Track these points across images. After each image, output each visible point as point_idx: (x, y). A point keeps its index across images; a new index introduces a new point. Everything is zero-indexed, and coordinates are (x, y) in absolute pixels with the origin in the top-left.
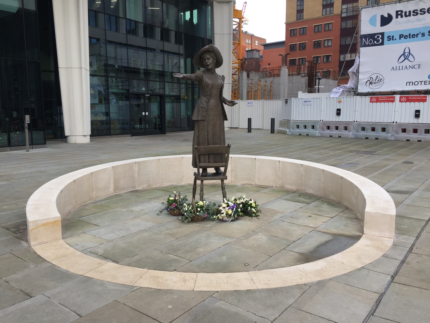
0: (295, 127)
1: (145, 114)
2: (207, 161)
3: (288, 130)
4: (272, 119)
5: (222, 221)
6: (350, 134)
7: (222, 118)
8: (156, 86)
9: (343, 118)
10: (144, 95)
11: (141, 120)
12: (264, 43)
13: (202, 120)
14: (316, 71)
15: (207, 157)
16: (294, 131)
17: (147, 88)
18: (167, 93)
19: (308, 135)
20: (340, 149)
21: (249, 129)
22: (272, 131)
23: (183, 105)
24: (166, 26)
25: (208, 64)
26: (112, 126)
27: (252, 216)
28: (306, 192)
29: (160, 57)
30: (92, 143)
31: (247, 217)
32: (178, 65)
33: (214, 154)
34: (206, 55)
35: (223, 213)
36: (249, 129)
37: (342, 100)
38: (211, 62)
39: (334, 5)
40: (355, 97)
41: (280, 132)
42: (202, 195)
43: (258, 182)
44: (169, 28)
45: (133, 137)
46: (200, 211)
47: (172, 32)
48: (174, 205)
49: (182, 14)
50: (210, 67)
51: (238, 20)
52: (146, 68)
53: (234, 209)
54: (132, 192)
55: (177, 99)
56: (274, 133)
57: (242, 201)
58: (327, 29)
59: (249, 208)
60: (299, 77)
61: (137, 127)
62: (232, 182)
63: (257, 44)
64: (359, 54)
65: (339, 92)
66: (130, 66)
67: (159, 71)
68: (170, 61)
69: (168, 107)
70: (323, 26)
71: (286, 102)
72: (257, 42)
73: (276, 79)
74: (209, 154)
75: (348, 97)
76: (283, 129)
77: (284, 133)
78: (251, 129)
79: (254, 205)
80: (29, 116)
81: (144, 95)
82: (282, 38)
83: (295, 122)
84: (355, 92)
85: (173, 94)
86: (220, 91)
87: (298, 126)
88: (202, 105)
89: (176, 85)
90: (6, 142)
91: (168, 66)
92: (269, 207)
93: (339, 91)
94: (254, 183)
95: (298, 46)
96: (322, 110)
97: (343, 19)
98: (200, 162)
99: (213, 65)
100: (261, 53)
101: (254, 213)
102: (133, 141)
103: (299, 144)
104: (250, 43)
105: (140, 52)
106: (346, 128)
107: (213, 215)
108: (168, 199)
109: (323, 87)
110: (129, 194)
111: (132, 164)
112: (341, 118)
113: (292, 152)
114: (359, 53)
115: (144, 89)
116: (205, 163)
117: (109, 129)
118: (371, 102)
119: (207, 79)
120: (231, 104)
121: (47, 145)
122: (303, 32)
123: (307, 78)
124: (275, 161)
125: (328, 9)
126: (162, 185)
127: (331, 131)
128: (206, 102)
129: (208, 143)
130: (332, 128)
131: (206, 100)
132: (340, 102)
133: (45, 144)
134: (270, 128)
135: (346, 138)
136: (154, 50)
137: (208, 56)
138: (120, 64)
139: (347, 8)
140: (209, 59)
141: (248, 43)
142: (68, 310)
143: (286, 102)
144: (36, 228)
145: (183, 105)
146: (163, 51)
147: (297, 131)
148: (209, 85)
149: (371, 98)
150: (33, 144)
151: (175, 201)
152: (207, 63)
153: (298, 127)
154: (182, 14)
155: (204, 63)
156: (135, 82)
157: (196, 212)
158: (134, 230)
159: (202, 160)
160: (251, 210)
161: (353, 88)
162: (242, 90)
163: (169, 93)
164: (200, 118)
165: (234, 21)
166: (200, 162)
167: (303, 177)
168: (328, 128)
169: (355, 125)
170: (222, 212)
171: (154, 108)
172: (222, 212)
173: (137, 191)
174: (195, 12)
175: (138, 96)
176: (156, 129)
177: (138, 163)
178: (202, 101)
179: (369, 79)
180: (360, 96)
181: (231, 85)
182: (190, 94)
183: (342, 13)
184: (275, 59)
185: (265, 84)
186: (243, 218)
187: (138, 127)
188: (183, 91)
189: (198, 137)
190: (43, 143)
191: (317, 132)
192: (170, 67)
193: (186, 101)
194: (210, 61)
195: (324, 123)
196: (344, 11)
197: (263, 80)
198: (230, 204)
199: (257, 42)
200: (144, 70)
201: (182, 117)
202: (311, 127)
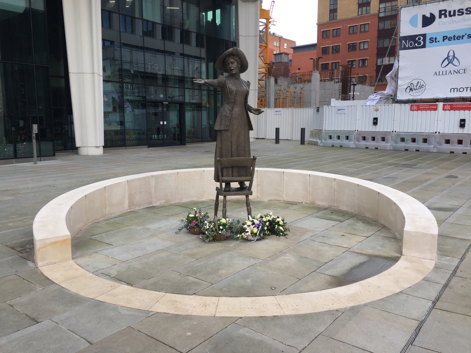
0: (328, 137)
1: (163, 123)
3: (319, 141)
4: (276, 128)
5: (247, 240)
6: (388, 145)
7: (247, 129)
8: (175, 93)
9: (380, 128)
11: (159, 130)
12: (293, 46)
13: (225, 130)
17: (165, 95)
18: (187, 100)
19: (341, 146)
20: (376, 162)
21: (277, 140)
22: (303, 142)
24: (186, 27)
25: (232, 68)
26: (127, 137)
27: (280, 235)
28: (339, 208)
29: (179, 61)
30: (105, 154)
31: (274, 236)
32: (199, 69)
33: (238, 167)
34: (230, 59)
35: (248, 232)
36: (277, 140)
37: (379, 108)
38: (235, 66)
40: (393, 104)
41: (311, 143)
42: (224, 212)
46: (222, 229)
47: (193, 34)
48: (194, 223)
49: (204, 14)
50: (234, 72)
51: (265, 21)
53: (260, 227)
55: (198, 107)
56: (304, 144)
58: (363, 30)
59: (277, 226)
62: (258, 197)
63: (285, 47)
66: (146, 71)
67: (179, 76)
68: (190, 66)
69: (188, 115)
70: (359, 27)
71: (318, 110)
72: (286, 45)
74: (232, 167)
75: (386, 105)
76: (314, 140)
77: (315, 144)
78: (279, 139)
79: (281, 223)
80: (37, 125)
81: (162, 103)
82: (314, 40)
84: (393, 99)
85: (194, 101)
87: (331, 136)
88: (225, 114)
89: (196, 92)
90: (12, 153)
92: (298, 225)
93: (376, 98)
95: (331, 49)
96: (439, 120)
98: (222, 176)
99: (237, 69)
100: (290, 57)
101: (282, 231)
103: (332, 157)
104: (278, 45)
105: (157, 56)
106: (383, 139)
107: (237, 233)
108: (188, 216)
109: (358, 93)
111: (148, 177)
114: (398, 56)
115: (162, 96)
117: (124, 140)
118: (411, 110)
119: (231, 85)
120: (257, 113)
121: (56, 157)
122: (337, 33)
123: (341, 84)
124: (305, 175)
125: (364, 8)
127: (367, 142)
128: (229, 110)
130: (368, 139)
131: (230, 108)
132: (377, 110)
133: (54, 155)
134: (299, 138)
135: (384, 150)
137: (232, 60)
138: (136, 69)
140: (232, 64)
141: (276, 46)
142: (77, 337)
143: (318, 110)
144: (44, 247)
145: (204, 114)
146: (182, 55)
150: (42, 155)
151: (195, 218)
152: (230, 68)
154: (204, 14)
155: (228, 67)
156: (152, 89)
157: (218, 230)
158: (151, 249)
160: (278, 228)
161: (392, 95)
162: (269, 98)
165: (261, 22)
166: (222, 176)
167: (336, 193)
170: (246, 231)
171: (173, 116)
172: (246, 231)
173: (153, 207)
174: (218, 12)
175: (156, 104)
176: (175, 139)
177: (156, 177)
178: (226, 109)
179: (409, 85)
180: (399, 103)
181: (257, 91)
183: (379, 13)
185: (294, 91)
186: (270, 237)
187: (156, 137)
188: (205, 98)
189: (221, 148)
190: (52, 155)
191: (351, 144)
192: (191, 72)
193: (208, 110)
194: (234, 66)
195: (359, 133)
196: (382, 10)
197: (292, 86)
198: (255, 222)
199: (286, 45)
200: (163, 75)
201: (203, 127)
202: (344, 137)
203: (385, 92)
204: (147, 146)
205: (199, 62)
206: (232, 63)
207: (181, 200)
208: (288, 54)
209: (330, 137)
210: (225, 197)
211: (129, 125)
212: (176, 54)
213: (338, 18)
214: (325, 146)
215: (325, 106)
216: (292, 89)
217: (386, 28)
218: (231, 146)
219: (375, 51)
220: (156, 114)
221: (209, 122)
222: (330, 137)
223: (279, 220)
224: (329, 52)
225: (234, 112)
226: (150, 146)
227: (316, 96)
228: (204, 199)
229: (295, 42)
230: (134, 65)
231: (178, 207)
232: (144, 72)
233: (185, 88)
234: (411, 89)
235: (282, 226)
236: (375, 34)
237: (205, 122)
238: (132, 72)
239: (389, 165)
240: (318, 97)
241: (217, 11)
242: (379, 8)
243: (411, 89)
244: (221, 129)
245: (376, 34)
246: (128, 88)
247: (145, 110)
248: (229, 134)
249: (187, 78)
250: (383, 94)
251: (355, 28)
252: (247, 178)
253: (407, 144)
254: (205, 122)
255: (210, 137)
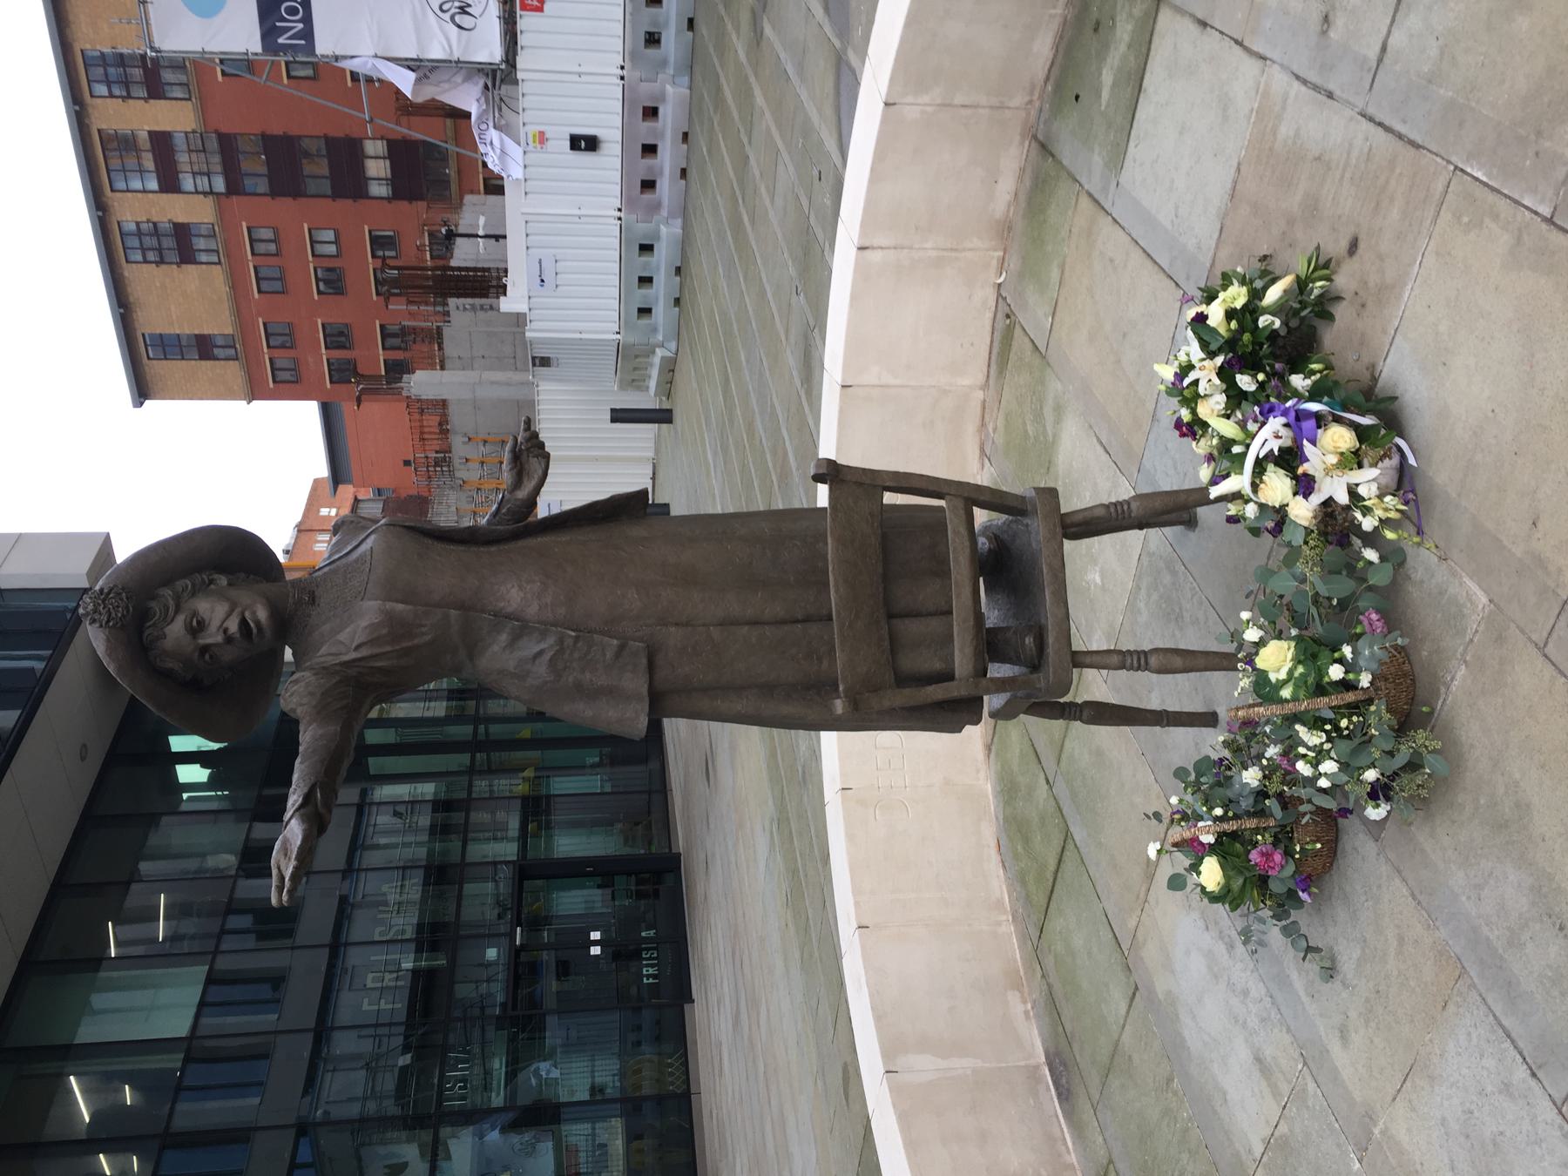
0: (644, 321)
1: (596, 943)
2: (935, 624)
3: (659, 352)
4: (613, 420)
6: (673, 95)
7: (636, 531)
8: (481, 899)
9: (609, 125)
10: (518, 952)
11: (622, 952)
12: (329, 486)
13: (651, 667)
14: (426, 269)
15: (911, 628)
16: (661, 329)
17: (491, 937)
18: (509, 850)
19: (678, 270)
20: (745, 95)
22: (662, 416)
23: (562, 785)
25: (233, 626)
26: (647, 1089)
29: (369, 885)
32: (401, 809)
34: (168, 643)
35: (1352, 492)
37: (532, 129)
38: (221, 609)
39: (181, 220)
40: (520, 75)
42: (1178, 661)
43: (973, 376)
44: (240, 846)
45: (695, 996)
46: (1349, 667)
48: (1267, 856)
49: (185, 796)
50: (262, 614)
52: (413, 946)
54: (1064, 1094)
55: (536, 809)
56: (670, 411)
57: (1206, 374)
59: (1263, 321)
60: (447, 332)
61: (654, 976)
64: (345, 57)
65: (502, 141)
66: (402, 1017)
67: (426, 883)
68: (383, 841)
69: (568, 845)
70: (261, 261)
71: (545, 362)
72: (324, 511)
73: (457, 419)
74: (891, 616)
75: (524, 103)
79: (1236, 296)
81: (518, 952)
82: (306, 414)
83: (624, 324)
84: (500, 78)
85: (514, 824)
86: (439, 546)
88: (541, 669)
89: (480, 817)
91: (405, 845)
93: (496, 143)
94: (980, 395)
95: (338, 354)
96: (577, 212)
97: (234, 188)
98: (947, 676)
99: (244, 596)
100: (366, 494)
102: (713, 998)
103: (723, 283)
106: (651, 113)
107: (1352, 568)
108: (1214, 898)
109: (482, 220)
110: (1087, 1114)
111: (897, 1092)
112: (610, 129)
113: (762, 294)
114: (337, 58)
115: (492, 953)
116: (950, 638)
117: (660, 1100)
118: (540, 9)
119: (349, 633)
120: (535, 464)
122: (283, 338)
123: (452, 302)
124: (862, 273)
125: (200, 243)
126: (1000, 902)
127: (661, 173)
128: (516, 638)
129: (807, 620)
130: (650, 169)
131: (504, 638)
132: (542, 138)
134: (649, 430)
135: (694, 108)
136: (343, 900)
137: (176, 630)
139: (194, 174)
143: (545, 362)
145: (562, 785)
146: (350, 870)
147: (662, 313)
148: (390, 619)
149: (524, 7)
151: (1225, 847)
152: (229, 639)
153: (645, 311)
154: (185, 796)
155: (228, 655)
156: (463, 991)
157: (1350, 697)
159: (929, 662)
160: (1275, 311)
161: (486, 87)
163: (512, 840)
164: (637, 683)
166: (947, 676)
168: (648, 185)
169: (637, 74)
170: (1343, 498)
171: (572, 901)
172: (1343, 498)
173: (1061, 1065)
174: (179, 743)
175: (522, 969)
176: (656, 894)
177: (891, 1050)
178: (514, 664)
179: (447, 16)
180: (515, 54)
182: (519, 755)
183: (211, 193)
184: (377, 422)
185: (477, 465)
187: (651, 971)
188: (502, 784)
189: (768, 689)
191: (667, 232)
192: (410, 838)
193: (545, 771)
194: (219, 613)
195: (628, 202)
196: (203, 183)
197: (461, 474)
198: (1275, 445)
199: (324, 511)
200: (419, 951)
201: (608, 789)
202: (644, 259)
203: (474, 109)
204: (686, 1007)
205: (374, 809)
206: (197, 627)
207: (999, 904)
208: (356, 500)
209: (646, 281)
210: (1081, 660)
211: (607, 1071)
212: (344, 892)
213: (229, 330)
214: (678, 332)
215: (528, 334)
216: (471, 474)
217: (264, 170)
218: (755, 623)
219: (346, 204)
220: (563, 970)
221: (593, 766)
222: (645, 311)
223: (1215, 314)
224: (348, 362)
225: (532, 610)
226: (683, 993)
227: (492, 383)
228: (987, 786)
229: (316, 481)
230: (384, 1049)
231: (1056, 924)
232: (410, 1024)
233: (463, 864)
234: (463, 10)
235: (1256, 295)
236: (285, 207)
237: (591, 783)
238: (405, 1060)
239: (758, 36)
240: (499, 376)
241: (174, 749)
242: (197, 192)
243: (463, 10)
244: (644, 690)
245: (286, 203)
246: (464, 1080)
247: (549, 1019)
248: (673, 637)
249: (430, 853)
250: (479, 117)
251: (263, 272)
252: (954, 525)
253: (667, 23)
254: (591, 783)
255: (645, 760)
